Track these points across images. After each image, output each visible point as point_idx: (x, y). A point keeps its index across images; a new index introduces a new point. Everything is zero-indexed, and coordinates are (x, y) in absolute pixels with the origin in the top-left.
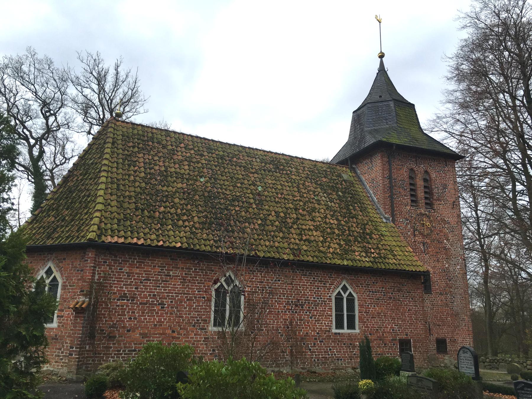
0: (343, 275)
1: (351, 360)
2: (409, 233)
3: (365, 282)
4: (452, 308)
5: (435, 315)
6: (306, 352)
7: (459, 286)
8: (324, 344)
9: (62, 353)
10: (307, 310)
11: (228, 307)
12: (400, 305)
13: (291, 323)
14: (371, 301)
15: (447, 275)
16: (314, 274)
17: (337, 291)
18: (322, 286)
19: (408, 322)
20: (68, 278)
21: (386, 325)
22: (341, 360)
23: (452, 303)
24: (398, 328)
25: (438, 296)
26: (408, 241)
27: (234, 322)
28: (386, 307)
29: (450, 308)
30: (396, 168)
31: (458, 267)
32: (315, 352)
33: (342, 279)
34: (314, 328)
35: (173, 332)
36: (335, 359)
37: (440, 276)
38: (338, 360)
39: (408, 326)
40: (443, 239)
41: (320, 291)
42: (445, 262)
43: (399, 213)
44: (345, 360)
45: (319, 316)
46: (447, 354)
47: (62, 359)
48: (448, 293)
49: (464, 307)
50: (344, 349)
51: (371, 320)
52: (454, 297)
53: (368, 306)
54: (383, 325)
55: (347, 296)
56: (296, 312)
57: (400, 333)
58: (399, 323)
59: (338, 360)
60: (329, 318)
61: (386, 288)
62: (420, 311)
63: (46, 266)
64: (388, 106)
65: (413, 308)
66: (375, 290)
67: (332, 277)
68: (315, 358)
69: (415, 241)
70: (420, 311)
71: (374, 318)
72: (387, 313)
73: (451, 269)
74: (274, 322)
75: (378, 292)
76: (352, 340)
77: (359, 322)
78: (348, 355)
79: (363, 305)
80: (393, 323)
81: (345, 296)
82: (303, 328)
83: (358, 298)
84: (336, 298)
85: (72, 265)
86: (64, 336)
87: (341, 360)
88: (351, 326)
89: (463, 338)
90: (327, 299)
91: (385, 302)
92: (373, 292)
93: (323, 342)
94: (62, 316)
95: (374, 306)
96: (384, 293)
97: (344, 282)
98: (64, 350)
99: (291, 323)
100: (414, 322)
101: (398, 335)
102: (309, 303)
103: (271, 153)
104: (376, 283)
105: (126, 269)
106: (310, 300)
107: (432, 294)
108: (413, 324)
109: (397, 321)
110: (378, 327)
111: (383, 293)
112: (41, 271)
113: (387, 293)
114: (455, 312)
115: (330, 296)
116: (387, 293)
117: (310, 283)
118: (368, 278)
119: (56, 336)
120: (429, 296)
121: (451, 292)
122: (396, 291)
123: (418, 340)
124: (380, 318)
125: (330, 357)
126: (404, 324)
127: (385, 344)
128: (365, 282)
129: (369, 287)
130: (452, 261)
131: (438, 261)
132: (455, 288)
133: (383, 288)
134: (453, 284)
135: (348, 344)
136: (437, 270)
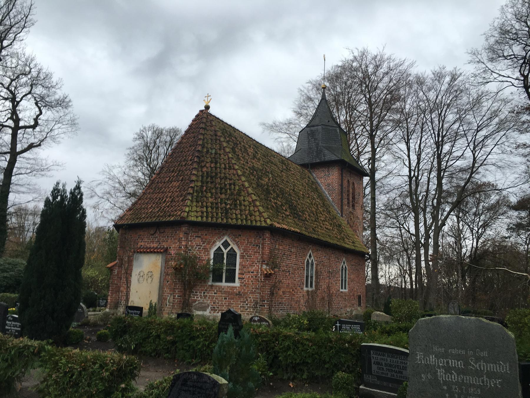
9: (246, 305)
13: (329, 285)
20: (245, 250)
33: (224, 235)
35: (293, 291)
47: (246, 309)
55: (228, 252)
63: (222, 239)
64: (336, 130)
81: (225, 252)
85: (248, 241)
86: (247, 293)
94: (244, 278)
98: (248, 302)
103: (227, 124)
112: (218, 243)
119: (239, 292)
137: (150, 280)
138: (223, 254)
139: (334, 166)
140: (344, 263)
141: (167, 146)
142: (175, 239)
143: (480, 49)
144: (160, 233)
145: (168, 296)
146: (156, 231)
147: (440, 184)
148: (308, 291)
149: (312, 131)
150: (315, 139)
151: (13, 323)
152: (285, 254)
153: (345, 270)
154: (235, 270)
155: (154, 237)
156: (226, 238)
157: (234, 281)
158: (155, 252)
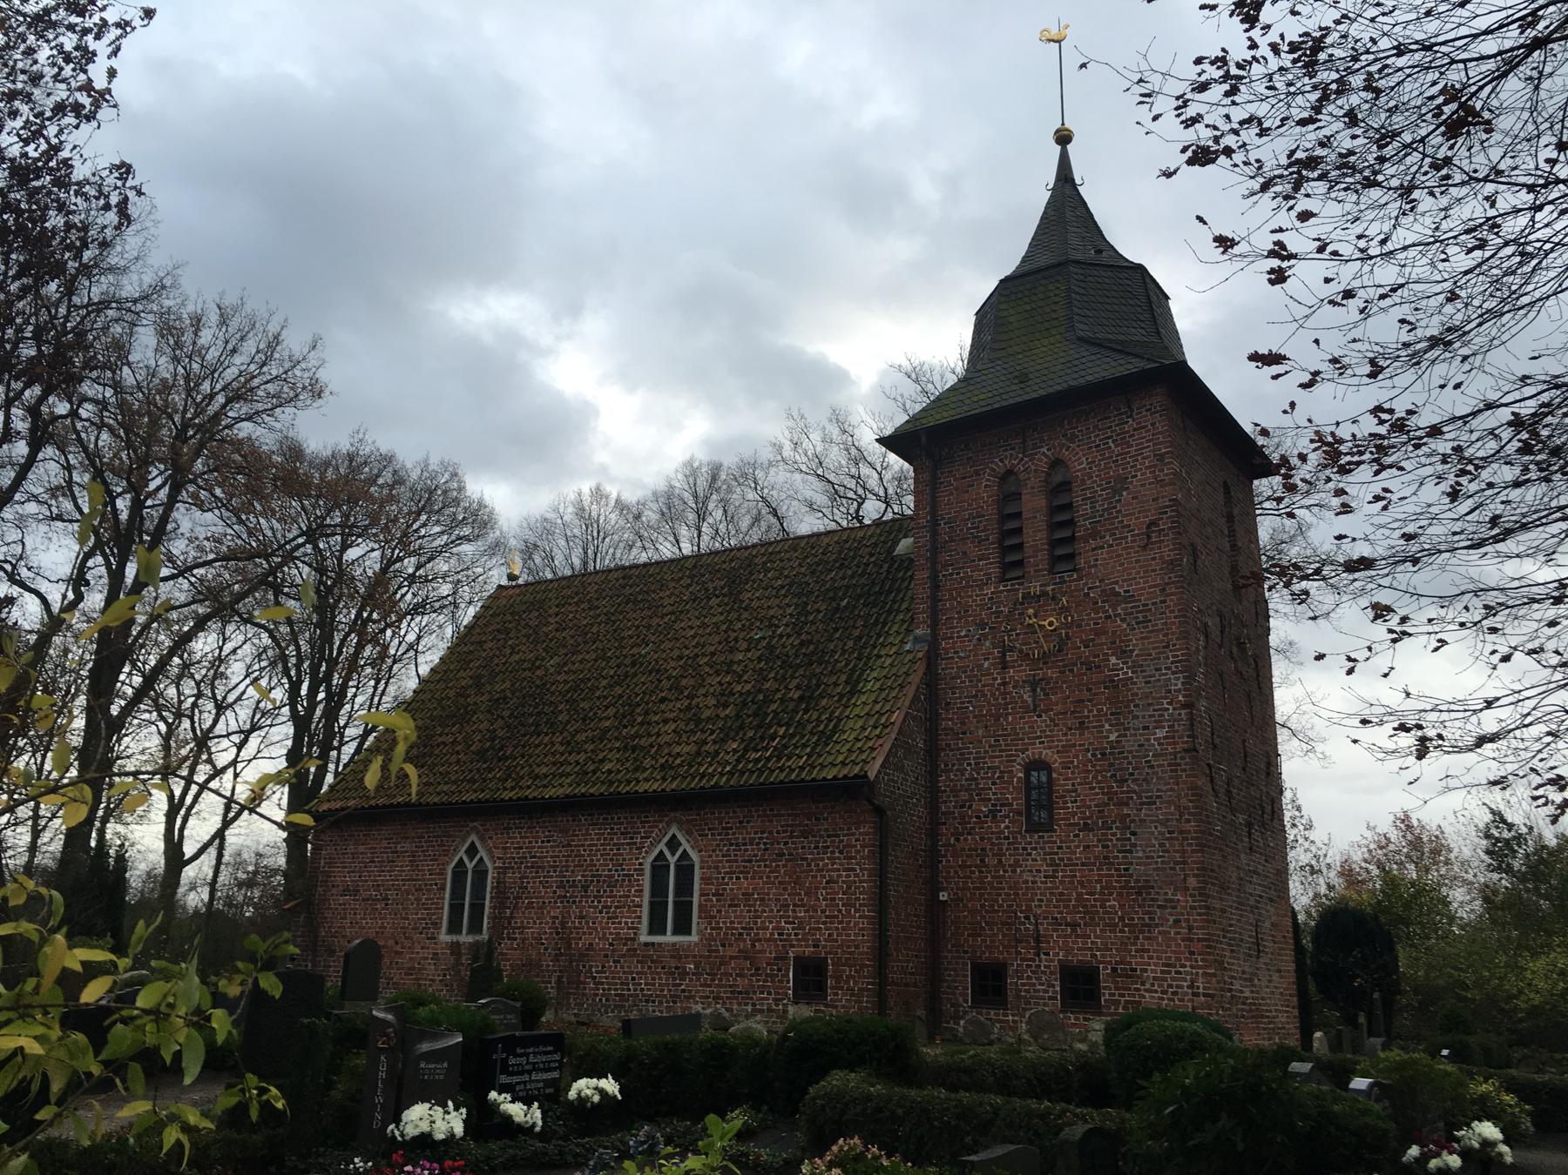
0: (672, 814)
1: (675, 1002)
2: (986, 665)
3: (720, 823)
4: (1125, 870)
5: (1061, 894)
6: (585, 983)
7: (1158, 797)
8: (622, 967)
10: (595, 897)
11: (467, 899)
12: (804, 871)
13: (563, 924)
14: (730, 867)
15: (1111, 765)
16: (612, 819)
17: (656, 852)
18: (628, 844)
19: (823, 911)
21: (763, 922)
22: (654, 1002)
23: (1126, 851)
24: (793, 929)
25: (1077, 836)
26: (983, 686)
27: (450, 922)
28: (768, 877)
29: (1116, 870)
30: (956, 489)
31: (1160, 733)
32: (603, 983)
34: (604, 934)
35: (397, 943)
36: (641, 1001)
37: (1088, 771)
38: (647, 1001)
39: (824, 923)
40: (1107, 654)
41: (622, 854)
42: (1107, 727)
43: (959, 613)
44: (661, 1003)
45: (616, 907)
46: (1101, 1014)
48: (1114, 822)
49: (1176, 863)
50: (660, 979)
51: (727, 912)
52: (1134, 834)
53: (723, 878)
54: (756, 923)
55: (655, 860)
56: (574, 902)
57: (798, 940)
58: (797, 917)
59: (647, 1001)
60: (635, 912)
61: (771, 833)
62: (861, 882)
65: (839, 876)
66: (744, 839)
67: (649, 822)
68: (602, 995)
69: (1004, 684)
70: (861, 882)
71: (736, 906)
72: (768, 894)
73: (1130, 744)
74: (535, 923)
75: (752, 844)
76: (680, 958)
77: (700, 917)
78: (670, 990)
79: (710, 878)
80: (781, 917)
81: (470, 866)
82: (584, 933)
83: (702, 861)
84: (653, 867)
87: (654, 1002)
88: (683, 927)
89: (1164, 965)
90: (635, 870)
91: (766, 866)
92: (737, 845)
93: (619, 962)
95: (738, 878)
96: (765, 844)
97: (674, 830)
99: (563, 924)
100: (840, 911)
101: (793, 946)
102: (598, 881)
104: (748, 822)
105: (351, 849)
106: (600, 876)
107: (1055, 831)
108: (837, 917)
109: (794, 911)
110: (743, 928)
111: (762, 846)
113: (772, 844)
114: (1137, 881)
115: (640, 864)
116: (772, 844)
117: (605, 839)
118: (727, 813)
120: (1040, 837)
121: (1123, 818)
122: (797, 837)
123: (847, 959)
124: (749, 906)
125: (631, 996)
126: (811, 917)
127: (757, 969)
128: (720, 823)
129: (728, 834)
130: (1136, 717)
131: (1082, 726)
132: (1142, 804)
133: (762, 833)
134: (1135, 792)
135: (670, 968)
136: (1076, 756)
138: (669, 866)
143: (513, 542)
147: (375, 688)
148: (455, 947)
152: (373, 862)
157: (689, 933)
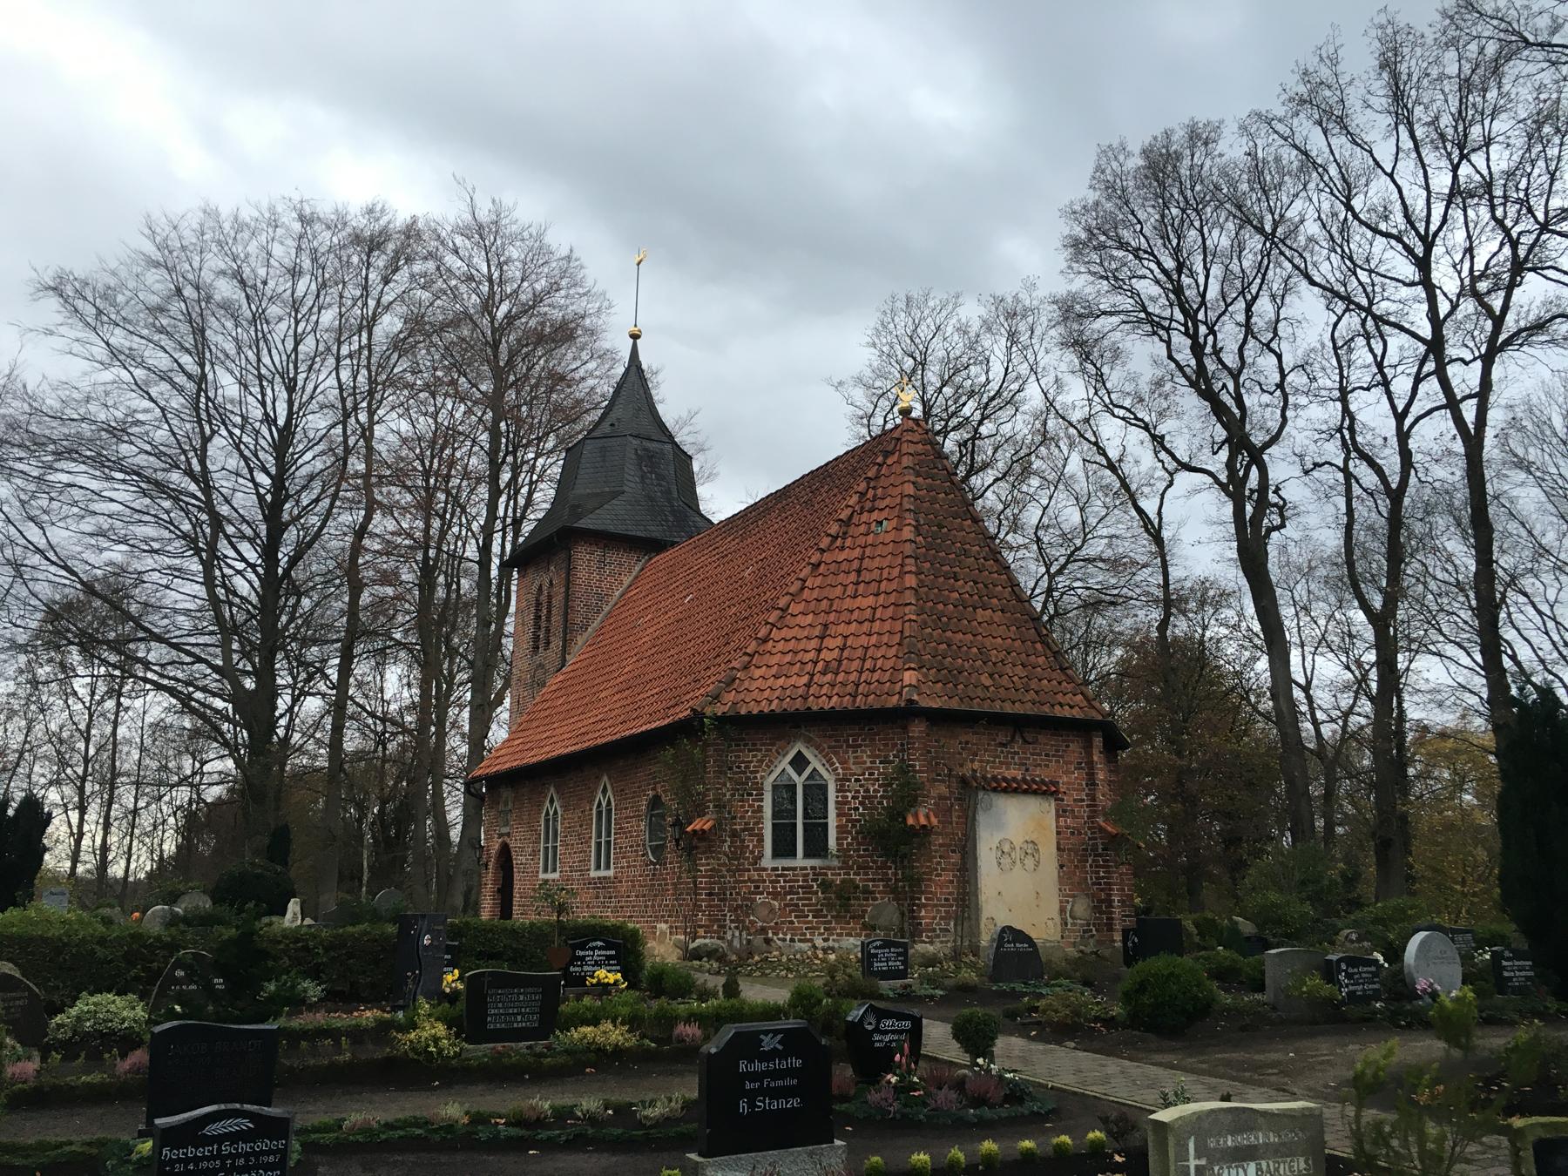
55: (807, 779)
81: (799, 781)
137: (1029, 862)
139: (618, 550)
140: (552, 801)
141: (256, 390)
142: (1066, 763)
144: (1026, 742)
145: (1068, 902)
146: (1013, 737)
149: (645, 449)
150: (660, 477)
151: (1517, 963)
153: (555, 820)
154: (795, 825)
155: (1009, 752)
156: (799, 746)
158: (1035, 793)
